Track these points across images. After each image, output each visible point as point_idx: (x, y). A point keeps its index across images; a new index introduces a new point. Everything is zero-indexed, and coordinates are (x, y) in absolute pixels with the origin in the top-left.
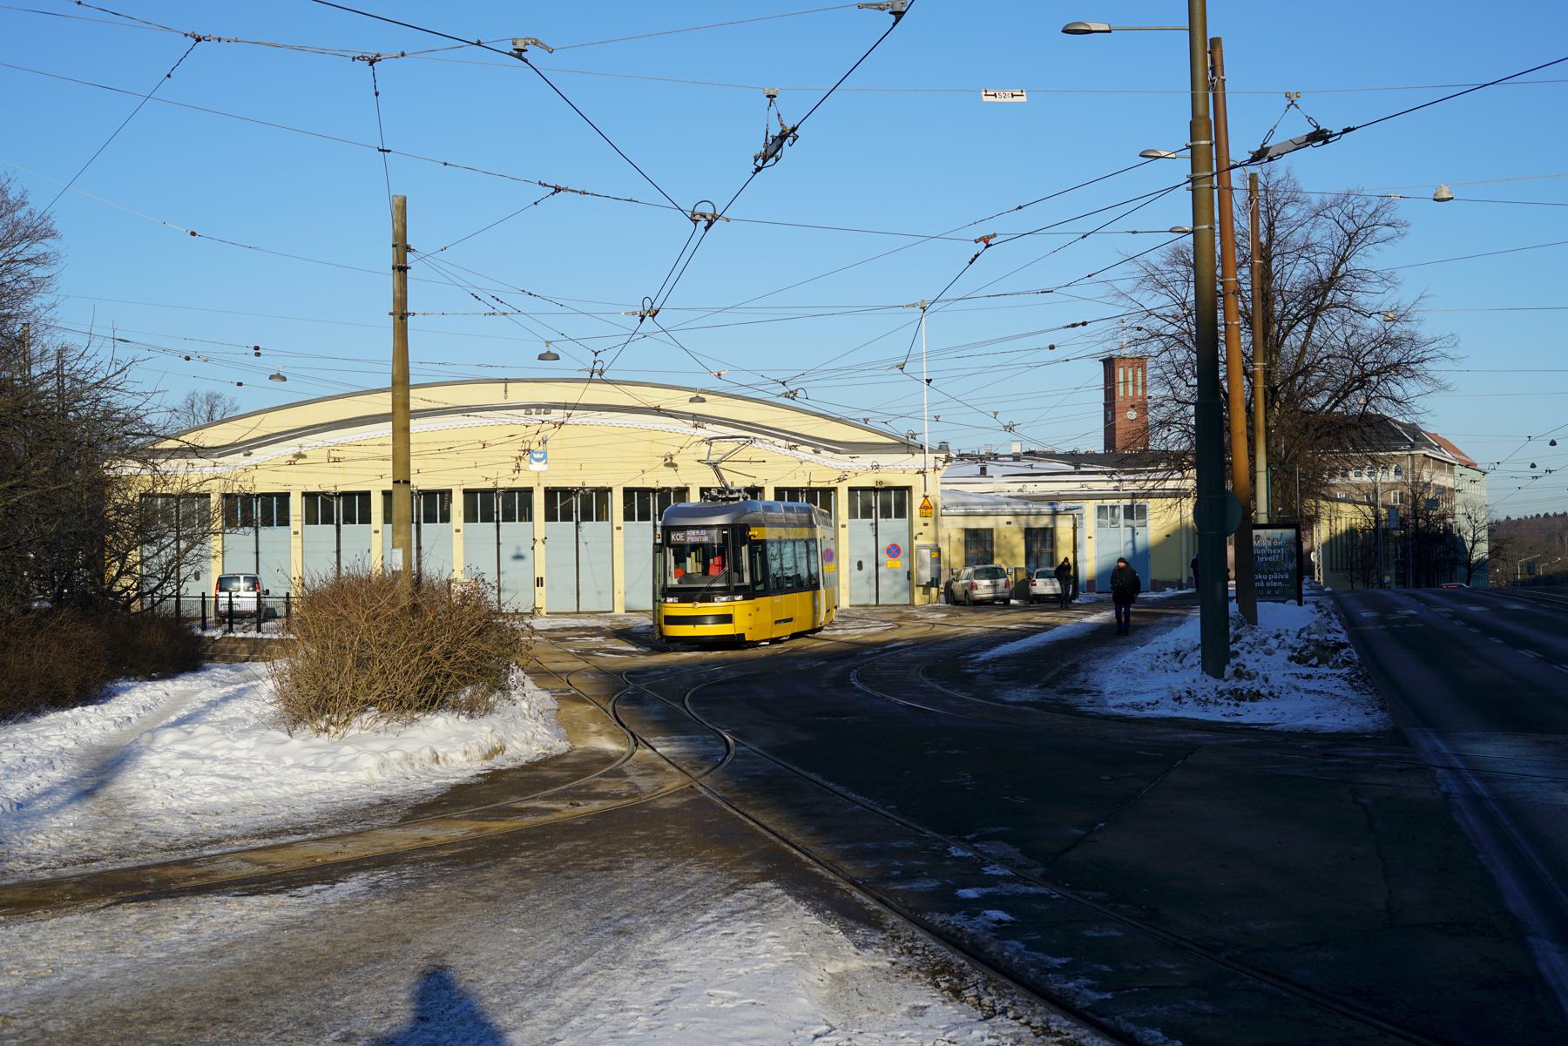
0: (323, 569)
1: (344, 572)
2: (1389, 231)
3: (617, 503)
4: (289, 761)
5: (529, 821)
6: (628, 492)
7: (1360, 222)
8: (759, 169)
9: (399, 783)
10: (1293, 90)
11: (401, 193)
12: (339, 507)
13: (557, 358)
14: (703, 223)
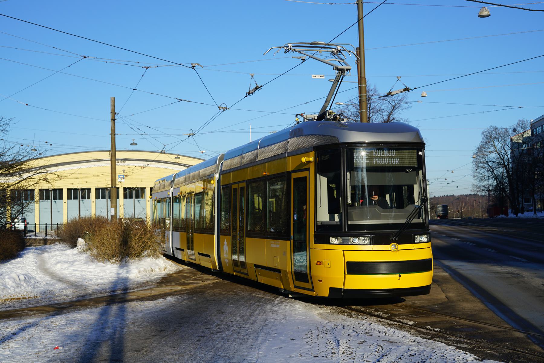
0: (74, 215)
1: (82, 216)
2: (406, 105)
4: (108, 272)
5: (195, 285)
7: (396, 102)
8: (246, 96)
9: (145, 277)
10: (399, 76)
11: (113, 96)
12: (51, 194)
13: (136, 144)
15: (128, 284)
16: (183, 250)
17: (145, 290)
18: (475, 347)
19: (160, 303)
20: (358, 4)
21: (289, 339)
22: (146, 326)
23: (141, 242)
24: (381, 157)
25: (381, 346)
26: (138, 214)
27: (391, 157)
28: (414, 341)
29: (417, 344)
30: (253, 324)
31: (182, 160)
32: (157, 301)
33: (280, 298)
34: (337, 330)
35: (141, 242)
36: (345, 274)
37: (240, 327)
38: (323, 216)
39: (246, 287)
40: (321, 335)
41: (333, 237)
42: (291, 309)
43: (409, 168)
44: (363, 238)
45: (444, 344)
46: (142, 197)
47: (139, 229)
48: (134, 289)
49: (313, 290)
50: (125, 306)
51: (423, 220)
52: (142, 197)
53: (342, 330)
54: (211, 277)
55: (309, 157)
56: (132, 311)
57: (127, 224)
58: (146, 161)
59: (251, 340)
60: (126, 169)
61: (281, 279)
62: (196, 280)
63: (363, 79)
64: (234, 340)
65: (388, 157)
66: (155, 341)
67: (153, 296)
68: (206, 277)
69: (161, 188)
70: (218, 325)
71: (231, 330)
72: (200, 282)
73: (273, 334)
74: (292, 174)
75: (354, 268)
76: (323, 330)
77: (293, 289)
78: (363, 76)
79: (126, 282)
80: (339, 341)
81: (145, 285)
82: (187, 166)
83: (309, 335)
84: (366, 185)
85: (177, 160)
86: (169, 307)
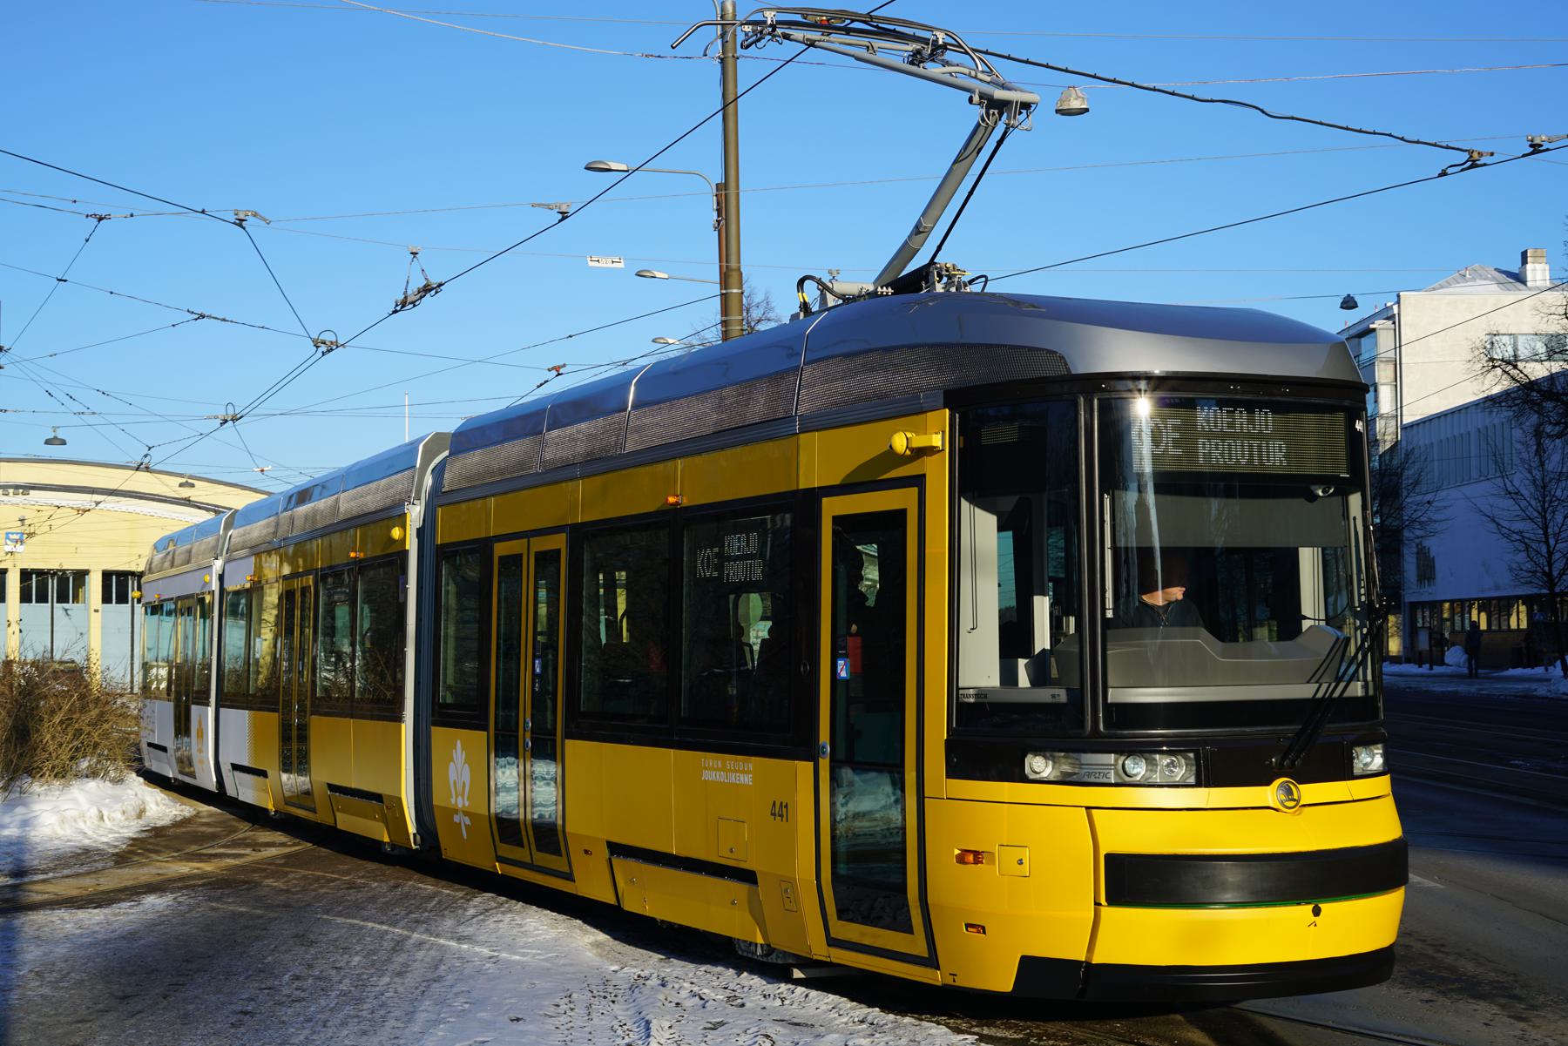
3: (94, 584)
5: (231, 862)
6: (107, 575)
13: (63, 443)
14: (323, 348)
15: (27, 857)
16: (263, 774)
17: (78, 875)
18: (1031, 1035)
19: (124, 915)
20: (722, 61)
21: (506, 1018)
22: (80, 983)
23: (71, 731)
24: (1223, 436)
25: (767, 1036)
26: (66, 649)
27: (1261, 436)
28: (862, 1022)
29: (870, 1031)
30: (400, 974)
31: (202, 492)
32: (115, 908)
33: (484, 899)
34: (646, 991)
35: (71, 731)
36: (1097, 904)
37: (361, 983)
38: (981, 668)
39: (384, 867)
40: (599, 1005)
41: (1037, 751)
42: (514, 932)
43: (1324, 481)
44: (1166, 760)
45: (944, 1029)
46: (76, 599)
47: (64, 694)
48: (44, 872)
49: (932, 961)
50: (17, 922)
51: (1366, 687)
52: (76, 599)
53: (658, 992)
54: (279, 837)
55: (922, 430)
56: (38, 937)
57: (29, 680)
58: (93, 491)
59: (392, 1023)
60: (30, 515)
61: (385, 820)
62: (235, 844)
63: (734, 275)
64: (344, 1024)
65: (1250, 436)
66: (104, 1027)
67: (103, 892)
68: (265, 836)
69: (177, 561)
70: (297, 978)
71: (334, 994)
72: (248, 851)
73: (458, 1004)
74: (826, 502)
75: (1136, 880)
76: (605, 990)
77: (819, 949)
78: (733, 264)
79: (21, 851)
80: (648, 1022)
81: (84, 858)
82: (216, 510)
83: (563, 1007)
84: (1157, 545)
85: (185, 493)
86: (151, 926)
